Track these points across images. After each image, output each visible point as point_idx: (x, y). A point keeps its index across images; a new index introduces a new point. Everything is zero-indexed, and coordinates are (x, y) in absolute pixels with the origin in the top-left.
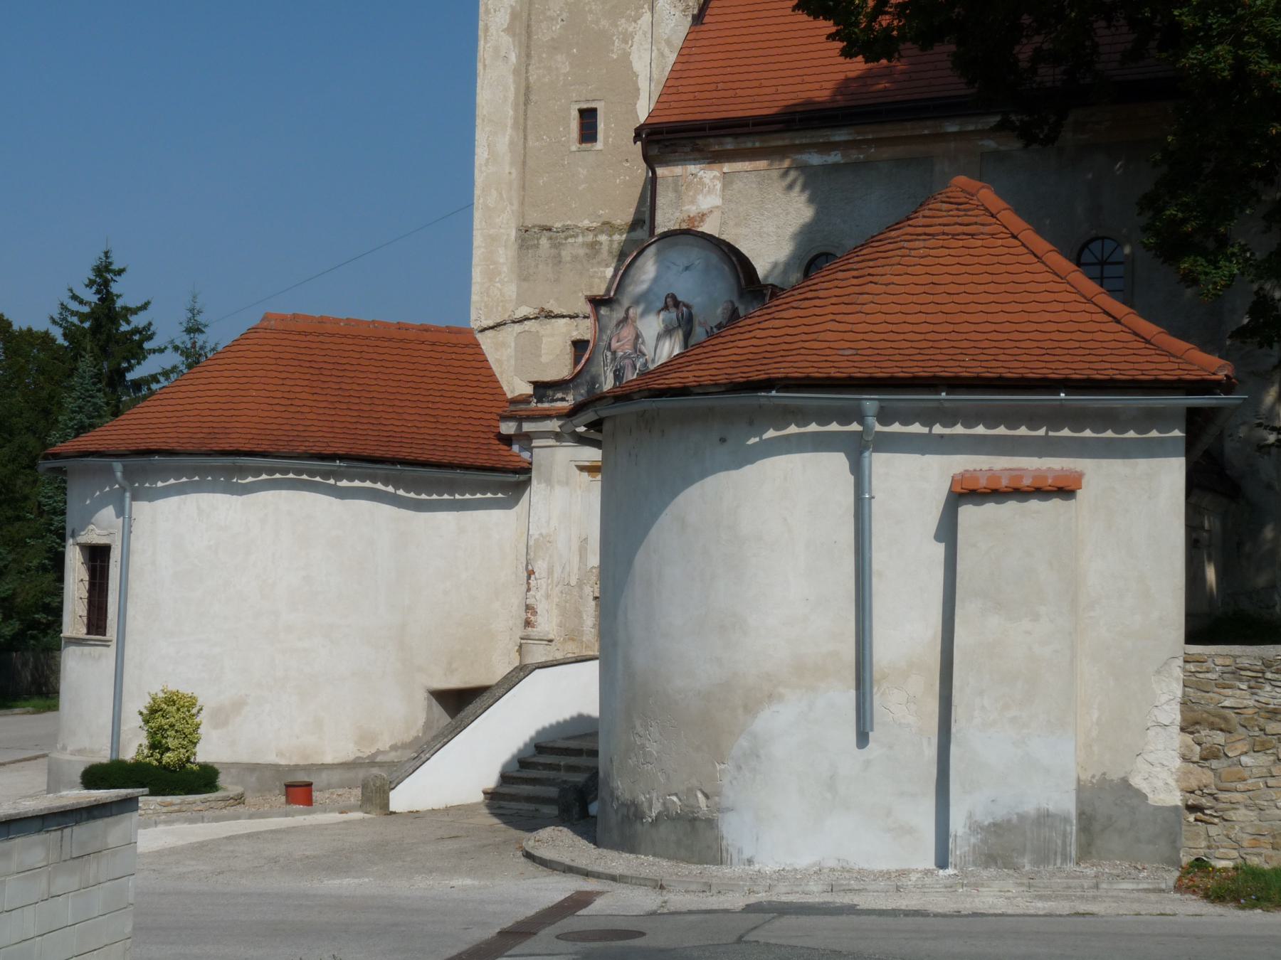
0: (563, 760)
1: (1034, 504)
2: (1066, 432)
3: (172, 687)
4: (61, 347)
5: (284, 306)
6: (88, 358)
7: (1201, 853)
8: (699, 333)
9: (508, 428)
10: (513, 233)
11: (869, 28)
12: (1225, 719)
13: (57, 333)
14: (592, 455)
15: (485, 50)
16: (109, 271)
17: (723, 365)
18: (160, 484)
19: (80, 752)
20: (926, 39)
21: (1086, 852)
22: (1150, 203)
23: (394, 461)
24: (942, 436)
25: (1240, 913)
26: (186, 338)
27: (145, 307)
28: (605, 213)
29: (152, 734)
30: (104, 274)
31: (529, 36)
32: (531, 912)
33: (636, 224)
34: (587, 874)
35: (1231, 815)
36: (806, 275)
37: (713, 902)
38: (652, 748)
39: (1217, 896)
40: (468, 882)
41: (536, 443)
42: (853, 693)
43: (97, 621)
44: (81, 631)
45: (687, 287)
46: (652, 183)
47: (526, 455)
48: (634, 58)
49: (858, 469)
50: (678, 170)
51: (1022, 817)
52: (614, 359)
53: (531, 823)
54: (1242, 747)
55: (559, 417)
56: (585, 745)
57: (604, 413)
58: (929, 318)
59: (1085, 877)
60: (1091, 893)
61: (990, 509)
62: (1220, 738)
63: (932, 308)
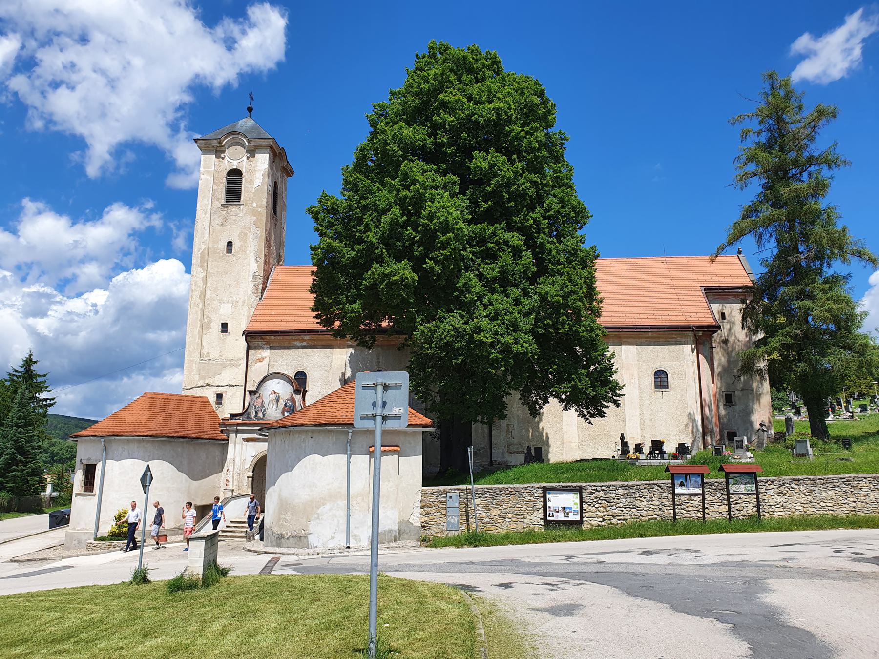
34: (276, 553)
52: (255, 408)
62: (429, 509)
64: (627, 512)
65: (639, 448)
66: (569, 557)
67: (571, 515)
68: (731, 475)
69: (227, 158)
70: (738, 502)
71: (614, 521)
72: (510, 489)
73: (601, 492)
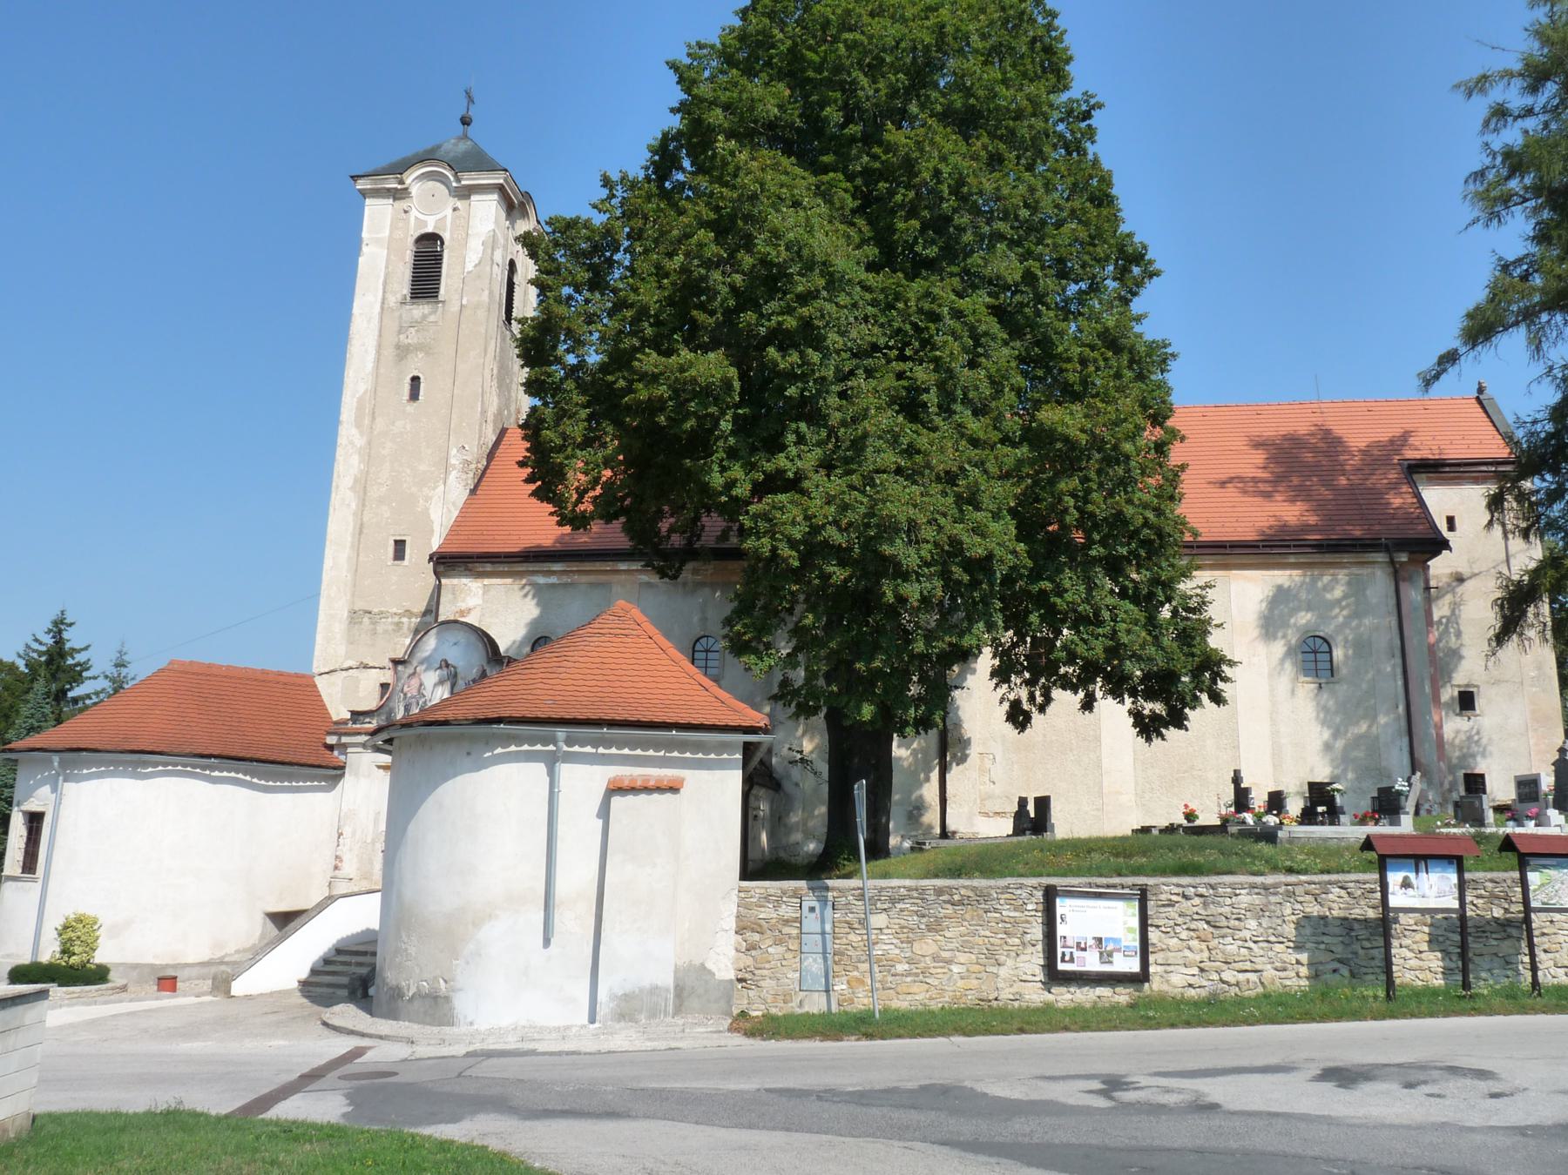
0: (354, 959)
1: (656, 796)
2: (676, 754)
3: (81, 911)
4: (22, 673)
5: (187, 655)
6: (42, 681)
7: (744, 1007)
8: (461, 684)
9: (331, 740)
10: (346, 614)
11: (573, 510)
12: (760, 926)
13: (21, 665)
14: (386, 759)
15: (335, 499)
16: (62, 623)
17: (484, 701)
18: (85, 771)
19: (8, 956)
20: (609, 518)
21: (678, 1010)
22: (728, 622)
23: (251, 760)
24: (603, 755)
25: (763, 1043)
26: (114, 670)
27: (86, 648)
28: (407, 605)
29: (64, 944)
30: (59, 626)
31: (365, 493)
32: (323, 1062)
33: (427, 612)
34: (363, 1035)
35: (762, 983)
36: (533, 650)
37: (445, 1051)
38: (412, 950)
39: (750, 1034)
40: (282, 1042)
41: (349, 750)
42: (542, 914)
43: (30, 864)
44: (18, 871)
45: (455, 656)
46: (439, 588)
47: (342, 758)
48: (431, 511)
49: (551, 773)
50: (455, 581)
51: (641, 990)
53: (327, 1001)
54: (769, 942)
55: (366, 734)
56: (369, 948)
57: (393, 735)
58: (599, 684)
59: (677, 1025)
60: (680, 1035)
61: (630, 799)
62: (756, 937)
63: (600, 677)
64: (1262, 953)
65: (1276, 801)
66: (1113, 1084)
67: (1117, 957)
68: (1533, 862)
69: (414, 213)
70: (1545, 931)
71: (1228, 976)
72: (963, 892)
73: (1197, 901)
